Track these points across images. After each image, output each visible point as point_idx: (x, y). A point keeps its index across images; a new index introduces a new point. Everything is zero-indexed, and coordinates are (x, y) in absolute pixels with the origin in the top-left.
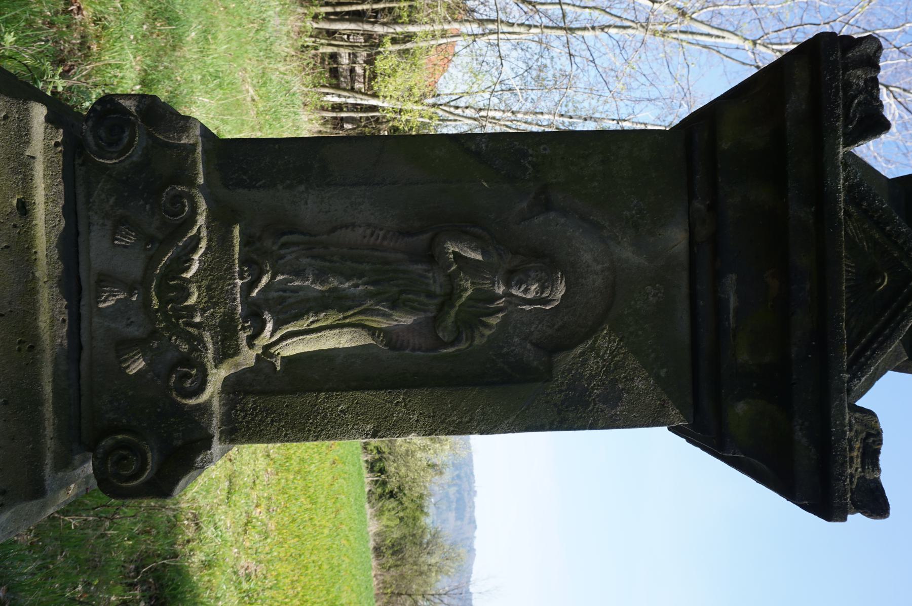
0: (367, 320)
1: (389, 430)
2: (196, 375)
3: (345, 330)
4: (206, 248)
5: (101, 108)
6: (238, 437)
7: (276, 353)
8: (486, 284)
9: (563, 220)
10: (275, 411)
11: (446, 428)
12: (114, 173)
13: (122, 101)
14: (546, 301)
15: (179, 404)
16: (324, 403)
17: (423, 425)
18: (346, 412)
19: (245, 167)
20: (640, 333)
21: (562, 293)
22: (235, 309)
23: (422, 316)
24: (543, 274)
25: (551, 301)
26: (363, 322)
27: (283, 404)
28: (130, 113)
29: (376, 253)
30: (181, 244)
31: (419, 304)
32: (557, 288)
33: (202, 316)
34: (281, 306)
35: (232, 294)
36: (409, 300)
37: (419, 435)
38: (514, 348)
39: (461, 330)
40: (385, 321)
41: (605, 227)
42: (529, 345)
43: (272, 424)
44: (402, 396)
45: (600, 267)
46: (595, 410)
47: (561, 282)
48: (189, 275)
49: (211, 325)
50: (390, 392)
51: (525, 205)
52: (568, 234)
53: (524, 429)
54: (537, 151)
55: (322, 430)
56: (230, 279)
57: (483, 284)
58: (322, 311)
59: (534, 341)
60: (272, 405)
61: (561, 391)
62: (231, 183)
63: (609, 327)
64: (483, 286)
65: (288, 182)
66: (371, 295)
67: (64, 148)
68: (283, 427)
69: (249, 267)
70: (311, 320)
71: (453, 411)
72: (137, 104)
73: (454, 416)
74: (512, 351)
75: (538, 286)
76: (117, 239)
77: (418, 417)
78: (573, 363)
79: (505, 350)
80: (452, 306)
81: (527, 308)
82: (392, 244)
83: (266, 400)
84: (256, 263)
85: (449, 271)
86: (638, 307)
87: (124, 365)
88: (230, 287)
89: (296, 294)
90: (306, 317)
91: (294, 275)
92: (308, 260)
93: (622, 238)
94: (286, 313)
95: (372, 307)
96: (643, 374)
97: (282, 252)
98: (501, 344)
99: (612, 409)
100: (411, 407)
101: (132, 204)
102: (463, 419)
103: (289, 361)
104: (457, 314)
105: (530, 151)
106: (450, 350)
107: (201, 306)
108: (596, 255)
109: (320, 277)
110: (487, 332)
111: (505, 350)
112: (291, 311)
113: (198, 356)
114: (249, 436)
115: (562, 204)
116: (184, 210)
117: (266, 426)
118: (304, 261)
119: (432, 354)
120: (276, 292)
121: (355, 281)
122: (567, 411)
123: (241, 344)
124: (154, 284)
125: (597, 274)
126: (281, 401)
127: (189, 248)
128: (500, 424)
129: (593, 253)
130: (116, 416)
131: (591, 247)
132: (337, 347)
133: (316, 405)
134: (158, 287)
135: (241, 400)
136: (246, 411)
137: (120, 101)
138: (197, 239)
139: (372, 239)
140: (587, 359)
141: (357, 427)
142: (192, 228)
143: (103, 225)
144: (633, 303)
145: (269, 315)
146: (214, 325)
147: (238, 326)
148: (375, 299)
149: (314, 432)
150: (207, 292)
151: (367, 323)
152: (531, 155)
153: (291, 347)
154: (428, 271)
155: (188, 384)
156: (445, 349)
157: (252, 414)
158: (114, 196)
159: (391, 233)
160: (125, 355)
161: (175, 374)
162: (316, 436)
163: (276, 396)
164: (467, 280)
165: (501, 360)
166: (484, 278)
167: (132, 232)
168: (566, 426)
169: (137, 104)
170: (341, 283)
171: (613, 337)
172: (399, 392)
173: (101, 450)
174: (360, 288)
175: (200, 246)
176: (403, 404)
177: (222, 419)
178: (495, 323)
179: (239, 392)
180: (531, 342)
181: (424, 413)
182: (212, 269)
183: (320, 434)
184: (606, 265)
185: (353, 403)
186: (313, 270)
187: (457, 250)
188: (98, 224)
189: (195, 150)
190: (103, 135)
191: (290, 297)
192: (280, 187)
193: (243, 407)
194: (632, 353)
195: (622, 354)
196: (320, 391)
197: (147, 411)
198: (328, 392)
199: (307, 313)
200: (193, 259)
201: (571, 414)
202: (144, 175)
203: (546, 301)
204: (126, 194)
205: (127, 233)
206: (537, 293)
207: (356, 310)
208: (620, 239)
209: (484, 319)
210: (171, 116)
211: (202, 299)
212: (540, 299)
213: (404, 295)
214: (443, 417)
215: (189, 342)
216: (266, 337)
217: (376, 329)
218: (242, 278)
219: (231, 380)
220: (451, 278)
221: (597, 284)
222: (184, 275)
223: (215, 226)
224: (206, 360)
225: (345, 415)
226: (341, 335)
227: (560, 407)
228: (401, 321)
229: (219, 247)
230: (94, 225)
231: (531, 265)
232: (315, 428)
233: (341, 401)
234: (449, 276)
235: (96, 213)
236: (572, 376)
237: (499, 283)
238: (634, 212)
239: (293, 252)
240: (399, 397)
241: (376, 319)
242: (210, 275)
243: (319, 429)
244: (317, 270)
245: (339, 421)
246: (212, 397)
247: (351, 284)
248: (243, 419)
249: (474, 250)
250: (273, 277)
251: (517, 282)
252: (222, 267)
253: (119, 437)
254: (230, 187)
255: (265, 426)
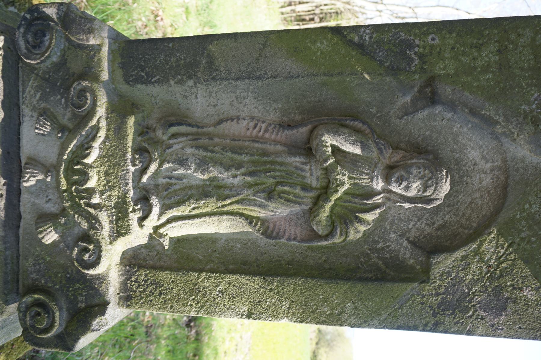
0: (245, 209)
1: (263, 313)
2: (93, 250)
3: (224, 217)
4: (105, 137)
5: (30, 17)
6: (132, 303)
7: (165, 233)
8: (364, 179)
9: (450, 115)
10: (163, 285)
11: (316, 318)
12: (40, 72)
13: (45, 10)
14: (429, 201)
15: (83, 273)
16: (205, 283)
17: (295, 312)
18: (224, 292)
19: (143, 64)
20: (533, 239)
21: (447, 192)
22: (127, 193)
23: (297, 208)
24: (427, 171)
25: (433, 200)
26: (241, 211)
27: (170, 280)
28: (53, 20)
29: (257, 145)
30: (83, 133)
31: (294, 197)
32: (441, 187)
33: (100, 197)
34: (167, 192)
35: (125, 179)
36: (284, 192)
37: (291, 321)
38: (390, 244)
39: (335, 224)
40: (262, 211)
41: (500, 122)
42: (406, 242)
43: (160, 297)
44: (275, 284)
45: (489, 165)
46: (475, 317)
47: (446, 181)
48: (89, 160)
49: (108, 206)
50: (264, 279)
51: (408, 98)
52: (455, 129)
53: (395, 327)
54: (424, 42)
55: (202, 307)
56: (123, 166)
57: (361, 179)
58: (202, 199)
59: (412, 239)
60: (161, 280)
61: (438, 294)
62: (131, 79)
63: (498, 231)
64: (361, 182)
65: (179, 77)
66: (250, 186)
67: (4, 52)
68: (169, 300)
69: (141, 155)
70: (192, 206)
71: (325, 302)
72: (57, 11)
73: (325, 307)
74: (388, 247)
75: (421, 184)
76: (37, 128)
77: (290, 304)
78: (453, 266)
79: (381, 245)
80: (327, 200)
81: (407, 205)
82: (273, 137)
83: (155, 275)
84: (147, 151)
85: (326, 165)
86: (533, 211)
87: (40, 236)
88: (123, 173)
89: (180, 182)
90: (187, 203)
91: (178, 164)
92: (192, 150)
93: (518, 135)
94: (170, 199)
95: (248, 197)
96: (534, 284)
97: (171, 142)
98: (377, 239)
99: (494, 318)
100: (283, 294)
101: (52, 98)
102: (334, 311)
103: (177, 242)
104: (332, 209)
105: (417, 42)
106: (324, 243)
107: (100, 189)
108: (485, 152)
109: (202, 165)
110: (362, 228)
111: (381, 245)
112: (174, 197)
113: (95, 233)
114: (142, 303)
115: (450, 97)
116: (86, 103)
117: (155, 297)
118: (189, 151)
119: (307, 245)
120: (163, 179)
121: (234, 171)
122: (444, 314)
123: (131, 225)
124: (63, 167)
125: (485, 173)
126: (167, 277)
127: (90, 137)
128: (371, 320)
129: (482, 150)
130: (38, 277)
131: (481, 143)
132: (218, 231)
133: (197, 284)
134: (66, 170)
135: (136, 272)
136: (139, 282)
137: (43, 9)
138: (96, 129)
139: (255, 131)
140: (469, 263)
141: (233, 307)
142: (91, 118)
143: (32, 116)
144: (527, 206)
145: (157, 200)
146: (110, 206)
147: (128, 209)
148: (252, 189)
149: (196, 308)
150: (105, 176)
151: (244, 212)
152: (418, 46)
153: (176, 229)
154: (305, 164)
155: (86, 257)
156: (319, 241)
157: (144, 285)
158: (39, 92)
159: (273, 126)
160: (41, 227)
161: (77, 248)
162: (197, 311)
163: (164, 272)
164: (344, 175)
165: (376, 255)
166: (362, 173)
167: (48, 122)
168: (441, 329)
169: (57, 11)
170: (220, 173)
171: (501, 242)
172: (273, 280)
173: (24, 305)
174: (239, 178)
175: (99, 135)
176: (276, 291)
177: (121, 287)
178: (371, 219)
179: (134, 265)
180: (408, 239)
181: (296, 302)
182: (109, 156)
183: (201, 309)
184: (496, 164)
185: (230, 285)
186: (195, 160)
187: (335, 143)
188: (28, 115)
189: (101, 50)
190: (31, 39)
191: (175, 184)
192: (172, 82)
193: (137, 279)
194: (522, 260)
195: (511, 260)
196: (201, 271)
197: (59, 275)
198: (208, 273)
199: (189, 199)
200: (93, 147)
201: (448, 318)
202: (62, 73)
203: (429, 201)
204: (48, 90)
205: (44, 124)
206: (419, 191)
207: (234, 199)
208: (515, 136)
209: (360, 215)
210: (80, 19)
211: (101, 183)
212: (421, 198)
213: (280, 187)
214: (314, 307)
215: (88, 221)
216: (152, 221)
217: (253, 217)
218: (134, 165)
219: (129, 253)
220: (327, 171)
221: (484, 183)
222: (85, 161)
223: (113, 117)
224: (101, 237)
225: (223, 295)
226: (220, 222)
227: (436, 310)
228: (277, 212)
229: (115, 136)
230: (25, 117)
231: (413, 161)
232: (196, 304)
233: (220, 282)
234: (326, 169)
235: (27, 106)
236: (451, 279)
237: (377, 179)
238: (534, 106)
239: (181, 142)
240: (272, 284)
241: (253, 208)
242: (107, 161)
243: (200, 305)
244: (199, 159)
245: (217, 300)
246: (109, 269)
247: (229, 174)
248: (137, 289)
249: (353, 143)
250: (160, 165)
251: (398, 178)
252: (117, 154)
253: (36, 296)
254: (131, 83)
255: (154, 297)
